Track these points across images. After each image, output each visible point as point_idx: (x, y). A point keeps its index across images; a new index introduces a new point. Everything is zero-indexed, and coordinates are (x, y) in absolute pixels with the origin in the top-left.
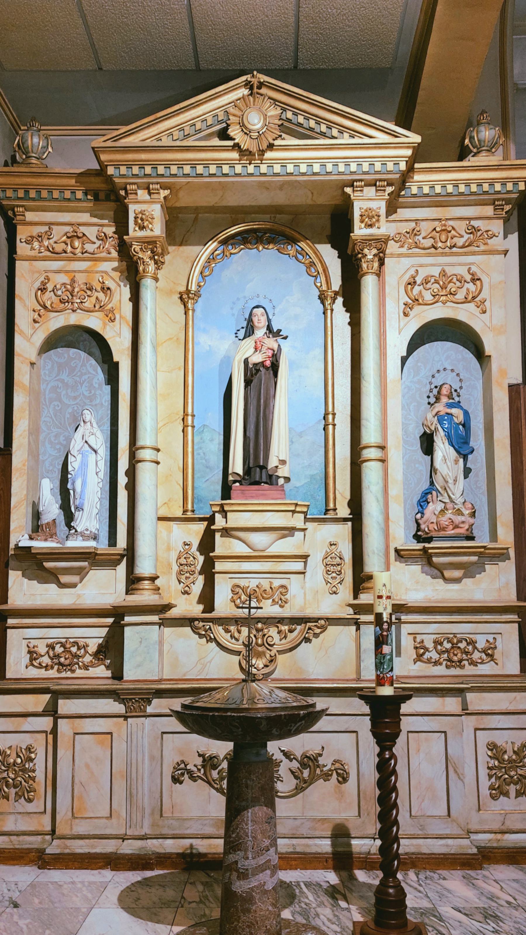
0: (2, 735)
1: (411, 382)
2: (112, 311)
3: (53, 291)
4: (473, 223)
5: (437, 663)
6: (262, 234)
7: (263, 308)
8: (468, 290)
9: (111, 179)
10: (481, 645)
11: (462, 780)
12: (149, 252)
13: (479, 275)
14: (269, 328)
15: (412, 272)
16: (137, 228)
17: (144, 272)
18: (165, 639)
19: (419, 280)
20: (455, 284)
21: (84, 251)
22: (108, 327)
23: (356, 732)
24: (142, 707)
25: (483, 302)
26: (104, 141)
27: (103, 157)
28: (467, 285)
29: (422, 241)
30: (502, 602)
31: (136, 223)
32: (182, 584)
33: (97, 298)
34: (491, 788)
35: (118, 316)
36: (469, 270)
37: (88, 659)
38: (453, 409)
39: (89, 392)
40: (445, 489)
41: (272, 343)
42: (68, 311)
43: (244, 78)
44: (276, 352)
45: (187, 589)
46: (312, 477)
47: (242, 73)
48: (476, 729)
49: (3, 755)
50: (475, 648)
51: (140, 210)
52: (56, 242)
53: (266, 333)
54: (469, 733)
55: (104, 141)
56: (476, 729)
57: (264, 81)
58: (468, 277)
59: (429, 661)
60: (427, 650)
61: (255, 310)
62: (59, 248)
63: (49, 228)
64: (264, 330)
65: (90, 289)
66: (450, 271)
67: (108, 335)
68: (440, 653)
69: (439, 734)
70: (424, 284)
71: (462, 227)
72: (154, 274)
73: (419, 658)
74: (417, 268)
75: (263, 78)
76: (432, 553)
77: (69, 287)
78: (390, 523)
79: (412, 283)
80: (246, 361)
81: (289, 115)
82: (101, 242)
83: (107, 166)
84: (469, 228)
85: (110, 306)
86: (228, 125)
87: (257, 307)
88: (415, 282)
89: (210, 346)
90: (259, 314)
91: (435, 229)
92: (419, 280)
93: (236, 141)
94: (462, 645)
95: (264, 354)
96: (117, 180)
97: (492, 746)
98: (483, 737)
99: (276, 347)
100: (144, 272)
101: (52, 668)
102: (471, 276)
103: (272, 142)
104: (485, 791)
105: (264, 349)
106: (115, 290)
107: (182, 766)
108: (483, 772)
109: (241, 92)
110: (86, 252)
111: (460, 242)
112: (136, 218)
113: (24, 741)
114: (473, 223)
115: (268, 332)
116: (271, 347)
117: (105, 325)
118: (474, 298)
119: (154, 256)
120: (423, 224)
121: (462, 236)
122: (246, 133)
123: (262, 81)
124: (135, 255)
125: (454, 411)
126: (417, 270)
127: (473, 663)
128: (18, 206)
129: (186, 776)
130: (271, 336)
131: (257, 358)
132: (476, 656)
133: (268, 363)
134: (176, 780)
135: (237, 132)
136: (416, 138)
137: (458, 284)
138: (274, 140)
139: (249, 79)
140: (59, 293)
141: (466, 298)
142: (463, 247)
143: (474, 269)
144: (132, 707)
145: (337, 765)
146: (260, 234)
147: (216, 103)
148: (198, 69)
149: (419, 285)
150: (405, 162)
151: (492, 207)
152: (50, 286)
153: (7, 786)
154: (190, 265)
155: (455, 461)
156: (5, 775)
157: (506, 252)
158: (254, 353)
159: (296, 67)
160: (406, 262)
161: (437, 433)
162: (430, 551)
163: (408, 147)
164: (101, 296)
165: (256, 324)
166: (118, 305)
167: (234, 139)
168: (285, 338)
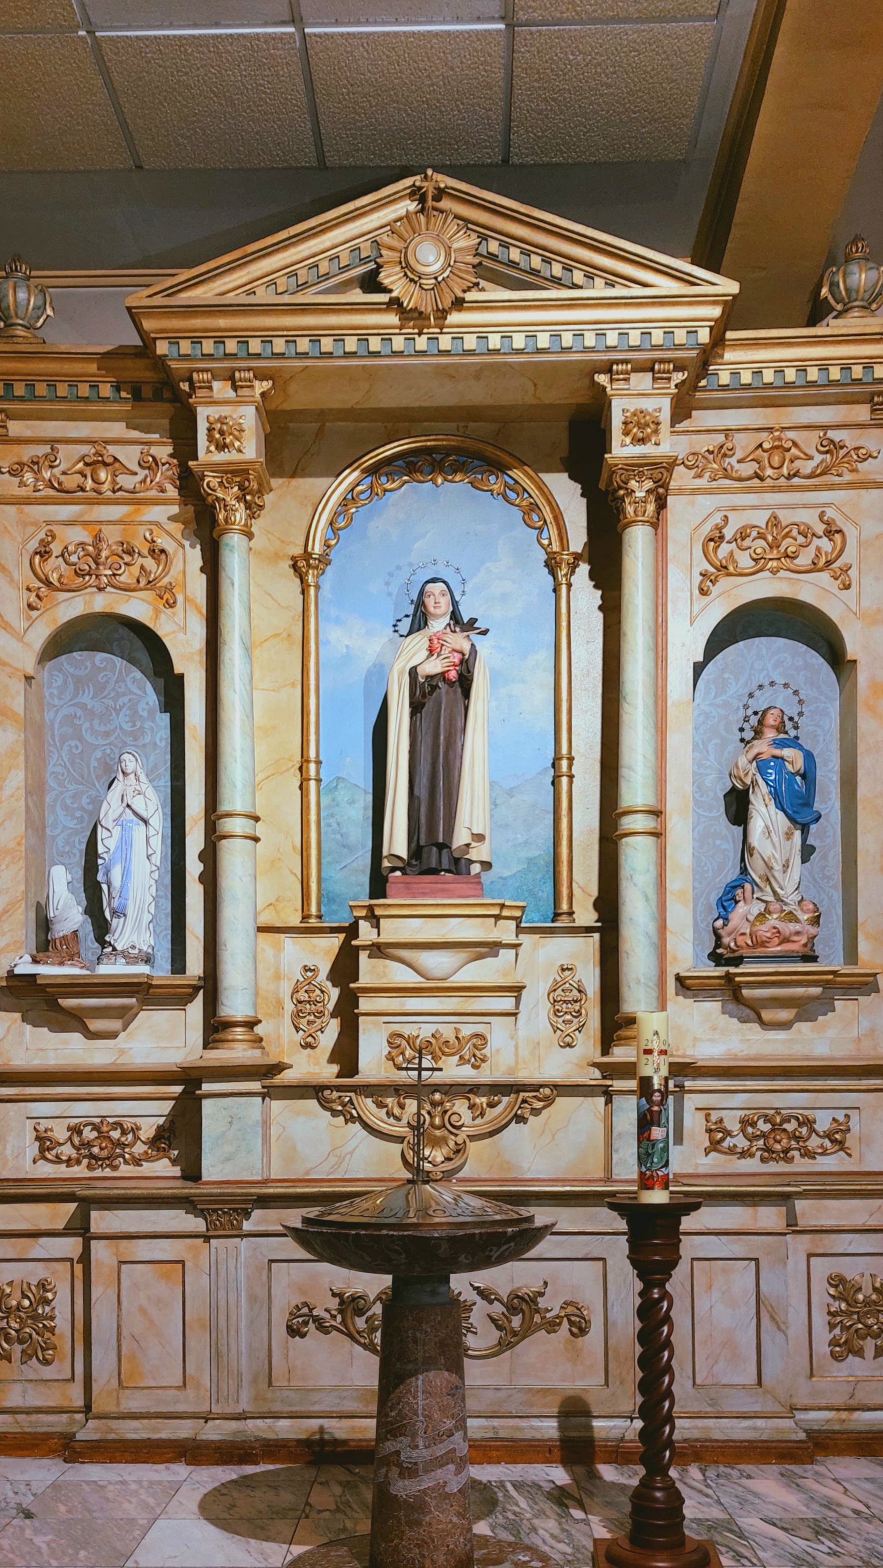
2: (170, 588)
3: (62, 555)
4: (831, 434)
5: (745, 1154)
7: (444, 582)
8: (818, 549)
9: (163, 362)
13: (840, 523)
14: (455, 616)
15: (717, 519)
16: (213, 448)
19: (729, 533)
20: (795, 540)
22: (163, 617)
25: (846, 570)
26: (150, 296)
27: (148, 324)
28: (816, 542)
31: (210, 438)
33: (142, 567)
34: (834, 1343)
35: (180, 598)
40: (768, 879)
41: (460, 641)
42: (89, 590)
43: (408, 182)
44: (467, 657)
46: (530, 861)
50: (812, 1130)
53: (449, 625)
55: (150, 296)
56: (810, 1256)
57: (446, 187)
58: (820, 528)
59: (732, 1151)
60: (728, 1133)
61: (430, 585)
63: (52, 449)
66: (785, 516)
68: (751, 1139)
77: (91, 548)
79: (716, 538)
80: (413, 673)
84: (825, 443)
85: (165, 581)
86: (379, 266)
87: (434, 580)
88: (722, 538)
89: (347, 646)
90: (437, 592)
91: (760, 445)
92: (729, 533)
93: (394, 294)
96: (174, 365)
97: (837, 1281)
98: (822, 1268)
99: (466, 647)
102: (825, 526)
103: (460, 294)
104: (822, 1347)
106: (176, 552)
107: (305, 1310)
108: (820, 1320)
110: (120, 489)
111: (807, 467)
112: (210, 430)
114: (831, 434)
115: (452, 623)
116: (457, 647)
117: (157, 612)
118: (829, 563)
119: (244, 496)
121: (811, 458)
122: (412, 280)
126: (726, 517)
127: (809, 1154)
129: (312, 1326)
130: (458, 629)
131: (434, 667)
132: (814, 1142)
133: (453, 675)
134: (294, 1331)
139: (418, 184)
140: (74, 559)
141: (814, 564)
143: (830, 513)
146: (438, 457)
148: (322, 166)
149: (728, 542)
150: (708, 329)
152: (56, 548)
153: (8, 1339)
154: (310, 510)
155: (787, 834)
158: (428, 658)
160: (707, 503)
161: (756, 789)
163: (715, 303)
164: (150, 563)
165: (431, 609)
166: (180, 578)
167: (390, 291)
168: (485, 633)
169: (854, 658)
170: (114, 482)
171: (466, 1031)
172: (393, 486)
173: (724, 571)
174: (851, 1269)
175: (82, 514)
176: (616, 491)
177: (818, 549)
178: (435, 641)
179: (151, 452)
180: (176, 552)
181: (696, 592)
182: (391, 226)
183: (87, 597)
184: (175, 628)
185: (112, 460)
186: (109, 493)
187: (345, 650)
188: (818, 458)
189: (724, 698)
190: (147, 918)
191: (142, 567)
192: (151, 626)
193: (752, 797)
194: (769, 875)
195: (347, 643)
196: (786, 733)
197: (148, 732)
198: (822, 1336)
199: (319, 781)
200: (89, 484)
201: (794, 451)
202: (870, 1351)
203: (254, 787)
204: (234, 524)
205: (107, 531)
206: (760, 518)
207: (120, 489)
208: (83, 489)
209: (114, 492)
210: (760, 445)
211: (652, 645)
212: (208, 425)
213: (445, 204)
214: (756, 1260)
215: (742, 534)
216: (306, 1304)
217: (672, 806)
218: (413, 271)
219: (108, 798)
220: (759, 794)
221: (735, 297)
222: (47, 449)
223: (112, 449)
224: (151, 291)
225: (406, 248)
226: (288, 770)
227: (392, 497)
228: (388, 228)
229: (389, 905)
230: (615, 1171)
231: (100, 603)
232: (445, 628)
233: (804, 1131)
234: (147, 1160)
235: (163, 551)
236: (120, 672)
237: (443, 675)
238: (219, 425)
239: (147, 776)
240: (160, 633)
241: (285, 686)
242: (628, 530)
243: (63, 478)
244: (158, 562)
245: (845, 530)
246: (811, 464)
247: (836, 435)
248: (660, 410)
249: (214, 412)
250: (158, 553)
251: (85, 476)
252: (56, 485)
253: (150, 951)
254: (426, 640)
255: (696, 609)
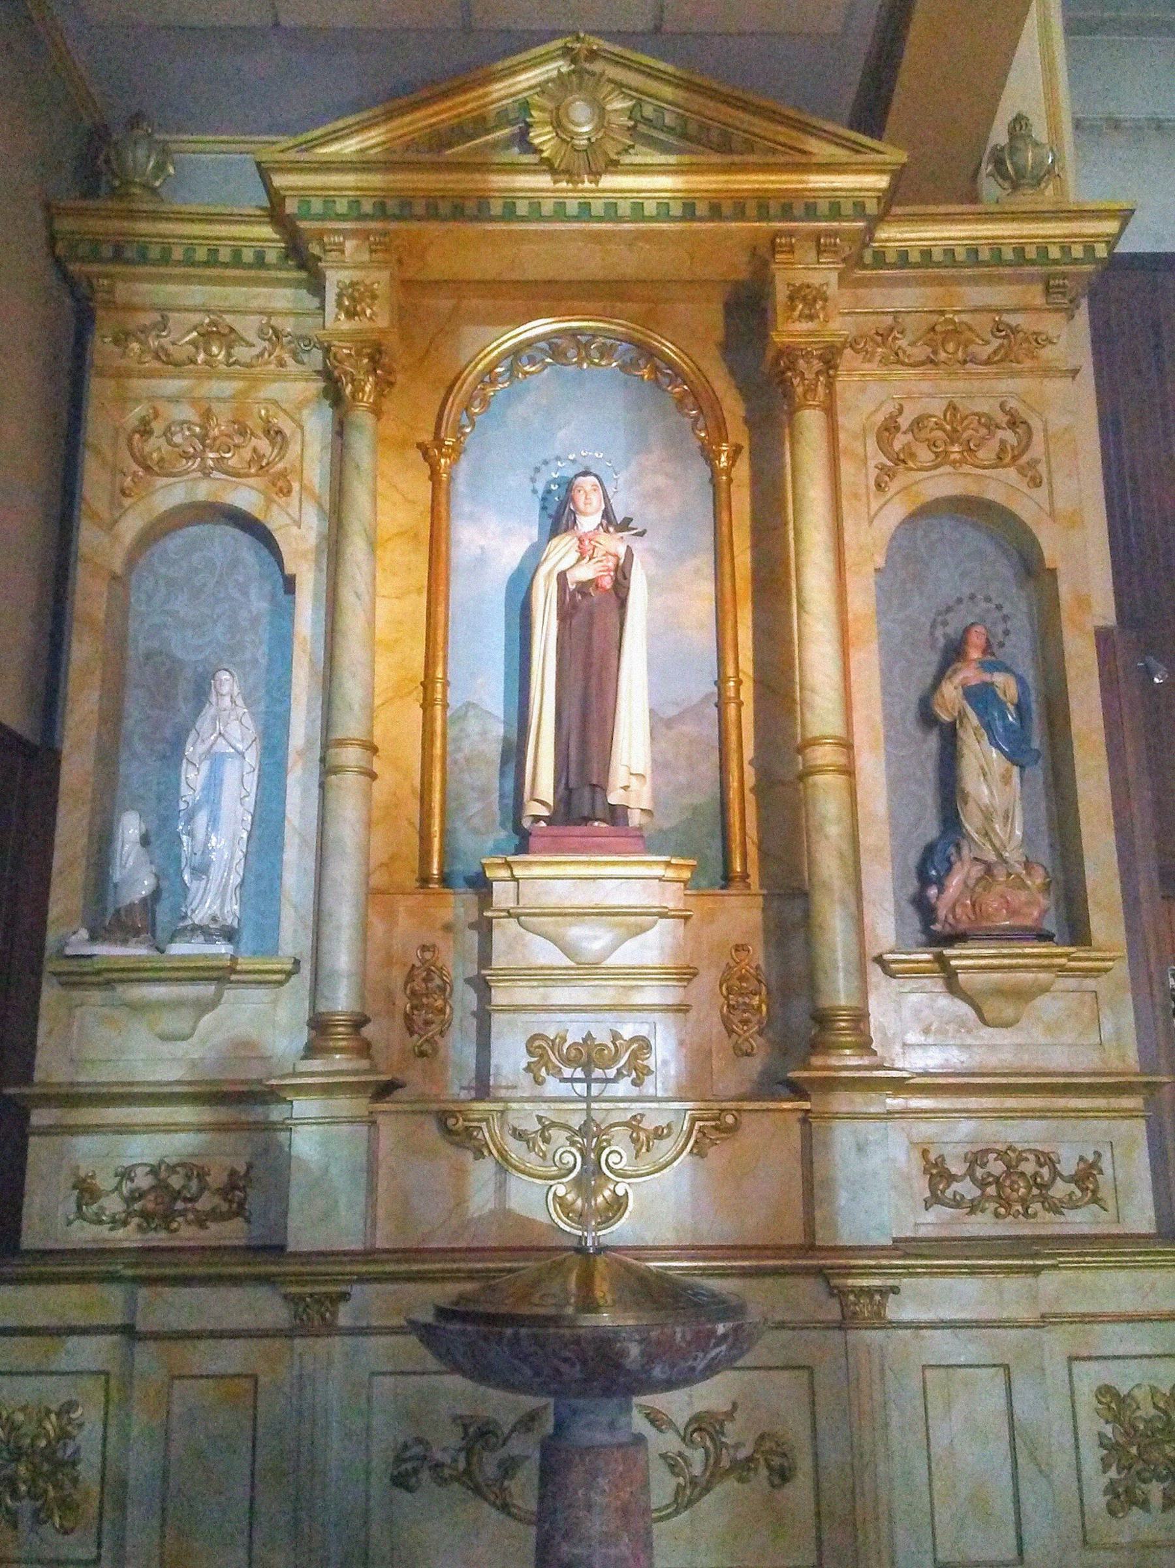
0: (5, 1380)
1: (893, 621)
2: (283, 474)
3: (165, 434)
4: (1006, 318)
5: (974, 1207)
6: (587, 338)
7: (596, 476)
8: (1003, 442)
9: (293, 223)
10: (1068, 1167)
11: (1047, 1477)
12: (366, 361)
13: (1024, 413)
14: (607, 514)
15: (890, 408)
16: (342, 317)
17: (353, 397)
18: (381, 1158)
19: (904, 422)
20: (977, 431)
21: (231, 360)
22: (275, 508)
23: (809, 1368)
24: (328, 1315)
25: (1033, 464)
26: (282, 151)
27: (279, 180)
28: (1000, 434)
29: (909, 350)
30: (1110, 1074)
31: (340, 305)
32: (416, 1036)
33: (255, 450)
34: (1111, 1489)
35: (296, 486)
36: (1002, 406)
37: (205, 1203)
38: (996, 674)
39: (229, 636)
40: (987, 834)
41: (616, 544)
42: (194, 475)
43: (559, 43)
44: (622, 561)
45: (426, 1047)
46: (695, 809)
47: (554, 35)
48: (1072, 1359)
49: (8, 1428)
50: (1055, 1174)
51: (347, 282)
52: (174, 343)
53: (601, 524)
54: (1056, 1368)
55: (282, 151)
56: (1072, 1359)
57: (599, 50)
58: (1003, 419)
59: (957, 1203)
60: (952, 1178)
61: (581, 479)
62: (179, 353)
63: (162, 317)
64: (597, 518)
65: (242, 432)
66: (966, 406)
67: (275, 521)
68: (982, 1184)
69: (993, 1370)
70: (916, 431)
71: (983, 323)
72: (374, 403)
73: (934, 1199)
74: (902, 402)
75: (597, 43)
76: (958, 967)
77: (198, 429)
78: (865, 904)
79: (890, 427)
80: (562, 577)
81: (648, 111)
82: (266, 344)
83: (284, 197)
84: (1001, 328)
85: (280, 466)
86: (529, 126)
87: (586, 473)
88: (897, 428)
89: (482, 548)
90: (588, 488)
91: (933, 329)
92: (904, 422)
93: (545, 155)
94: (1029, 1167)
95: (600, 564)
96: (303, 224)
97: (1105, 1391)
98: (1089, 1377)
99: (622, 551)
100: (353, 397)
101: (125, 1223)
102: (1008, 417)
103: (615, 157)
104: (1097, 1500)
105: (599, 553)
106: (293, 434)
107: (417, 1450)
108: (1092, 1456)
109: (554, 69)
110: (235, 363)
111: (985, 352)
112: (340, 296)
113: (55, 1392)
114: (1006, 318)
115: (605, 522)
116: (612, 551)
117: (269, 501)
118: (1015, 458)
119: (375, 370)
120: (909, 319)
121: (987, 343)
122: (563, 140)
123: (595, 48)
124: (336, 367)
125: (999, 679)
126: (901, 406)
127: (1055, 1208)
128: (100, 275)
129: (425, 1475)
130: (611, 529)
131: (585, 573)
132: (1060, 1190)
133: (607, 583)
134: (401, 1481)
135: (549, 137)
136: (897, 156)
137: (983, 431)
138: (618, 153)
139: (569, 45)
140: (178, 439)
141: (1000, 458)
142: (988, 362)
143: (1012, 404)
144: (305, 1317)
145: (768, 1445)
146: (583, 339)
147: (505, 87)
148: (468, 29)
149: (905, 433)
150: (875, 200)
151: (1039, 288)
152: (158, 427)
153: (15, 1494)
154: (442, 392)
155: (1003, 777)
156: (8, 1472)
157: (1075, 372)
158: (579, 561)
159: (657, 30)
160: (876, 391)
161: (965, 721)
162: (953, 963)
163: (882, 172)
164: (263, 445)
165: (581, 505)
166: (297, 464)
167: (542, 151)
168: (641, 534)
169: (1052, 566)
170: (229, 355)
171: (627, 1032)
172: (533, 369)
173: (902, 466)
174: (1125, 1378)
175: (191, 390)
176: (783, 373)
177: (1003, 442)
178: (587, 542)
179: (273, 322)
180: (293, 434)
181: (873, 487)
182: (542, 88)
183: (190, 484)
184: (289, 521)
185: (226, 331)
186: (223, 367)
187: (479, 551)
188: (996, 343)
189: (907, 613)
190: (235, 879)
191: (255, 450)
192: (261, 518)
193: (961, 732)
194: (987, 828)
195: (482, 542)
196: (993, 654)
197: (249, 645)
198: (1097, 1481)
199: (445, 706)
200: (201, 357)
201: (968, 334)
202: (1156, 1499)
203: (371, 713)
204: (362, 401)
205: (216, 407)
206: (937, 407)
207: (235, 363)
208: (194, 362)
209: (229, 365)
210: (933, 329)
211: (339, 638)
212: (337, 290)
213: (597, 67)
214: (1006, 1367)
215: (918, 423)
216: (419, 1441)
217: (860, 739)
218: (565, 130)
219: (197, 726)
220: (968, 727)
221: (904, 165)
222: (157, 317)
223: (228, 319)
224: (278, 147)
225: (558, 109)
226: (410, 693)
227: (534, 381)
228: (539, 89)
229: (531, 863)
230: (819, 1235)
231: (203, 491)
232: (597, 528)
233: (1045, 1171)
234: (215, 1220)
235: (279, 432)
236: (221, 575)
237: (594, 582)
238: (350, 290)
239: (244, 700)
240: (270, 526)
241: (409, 592)
242: (799, 414)
243: (171, 348)
244: (273, 444)
245: (1030, 422)
246: (989, 349)
247: (1011, 319)
248: (827, 284)
249: (345, 276)
250: (275, 435)
251: (197, 348)
252: (164, 358)
253: (235, 924)
254: (575, 541)
255: (874, 506)
